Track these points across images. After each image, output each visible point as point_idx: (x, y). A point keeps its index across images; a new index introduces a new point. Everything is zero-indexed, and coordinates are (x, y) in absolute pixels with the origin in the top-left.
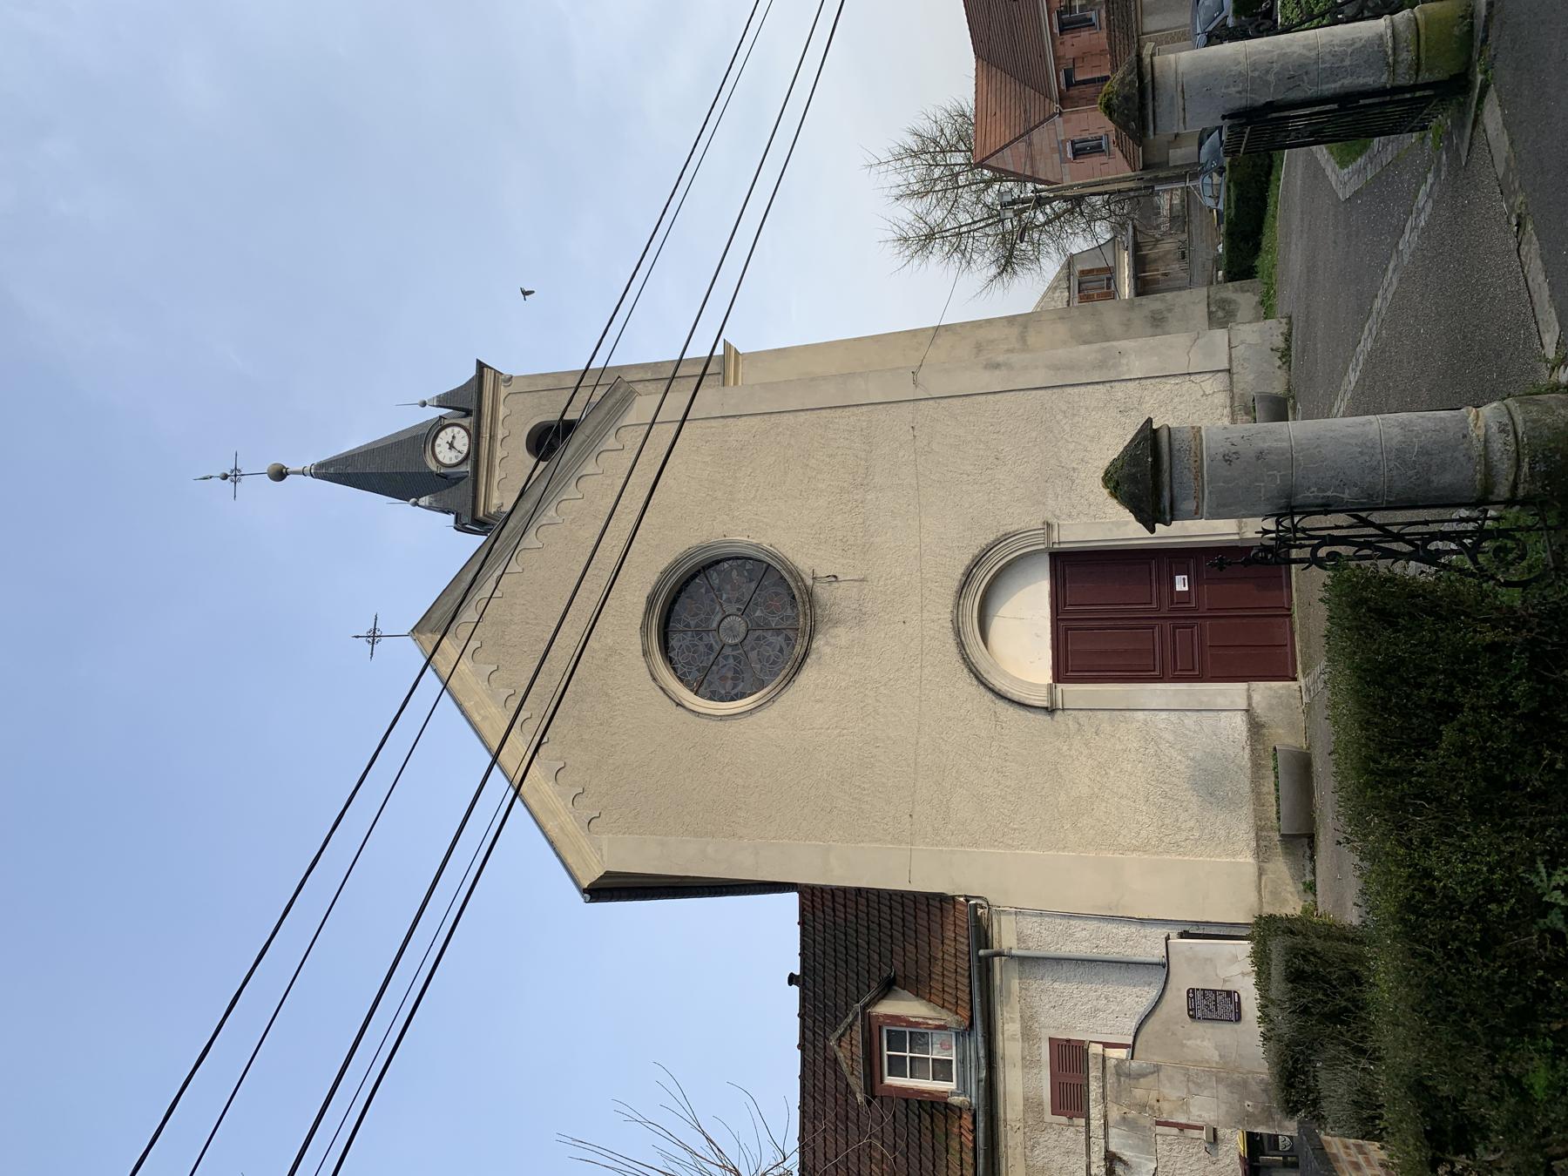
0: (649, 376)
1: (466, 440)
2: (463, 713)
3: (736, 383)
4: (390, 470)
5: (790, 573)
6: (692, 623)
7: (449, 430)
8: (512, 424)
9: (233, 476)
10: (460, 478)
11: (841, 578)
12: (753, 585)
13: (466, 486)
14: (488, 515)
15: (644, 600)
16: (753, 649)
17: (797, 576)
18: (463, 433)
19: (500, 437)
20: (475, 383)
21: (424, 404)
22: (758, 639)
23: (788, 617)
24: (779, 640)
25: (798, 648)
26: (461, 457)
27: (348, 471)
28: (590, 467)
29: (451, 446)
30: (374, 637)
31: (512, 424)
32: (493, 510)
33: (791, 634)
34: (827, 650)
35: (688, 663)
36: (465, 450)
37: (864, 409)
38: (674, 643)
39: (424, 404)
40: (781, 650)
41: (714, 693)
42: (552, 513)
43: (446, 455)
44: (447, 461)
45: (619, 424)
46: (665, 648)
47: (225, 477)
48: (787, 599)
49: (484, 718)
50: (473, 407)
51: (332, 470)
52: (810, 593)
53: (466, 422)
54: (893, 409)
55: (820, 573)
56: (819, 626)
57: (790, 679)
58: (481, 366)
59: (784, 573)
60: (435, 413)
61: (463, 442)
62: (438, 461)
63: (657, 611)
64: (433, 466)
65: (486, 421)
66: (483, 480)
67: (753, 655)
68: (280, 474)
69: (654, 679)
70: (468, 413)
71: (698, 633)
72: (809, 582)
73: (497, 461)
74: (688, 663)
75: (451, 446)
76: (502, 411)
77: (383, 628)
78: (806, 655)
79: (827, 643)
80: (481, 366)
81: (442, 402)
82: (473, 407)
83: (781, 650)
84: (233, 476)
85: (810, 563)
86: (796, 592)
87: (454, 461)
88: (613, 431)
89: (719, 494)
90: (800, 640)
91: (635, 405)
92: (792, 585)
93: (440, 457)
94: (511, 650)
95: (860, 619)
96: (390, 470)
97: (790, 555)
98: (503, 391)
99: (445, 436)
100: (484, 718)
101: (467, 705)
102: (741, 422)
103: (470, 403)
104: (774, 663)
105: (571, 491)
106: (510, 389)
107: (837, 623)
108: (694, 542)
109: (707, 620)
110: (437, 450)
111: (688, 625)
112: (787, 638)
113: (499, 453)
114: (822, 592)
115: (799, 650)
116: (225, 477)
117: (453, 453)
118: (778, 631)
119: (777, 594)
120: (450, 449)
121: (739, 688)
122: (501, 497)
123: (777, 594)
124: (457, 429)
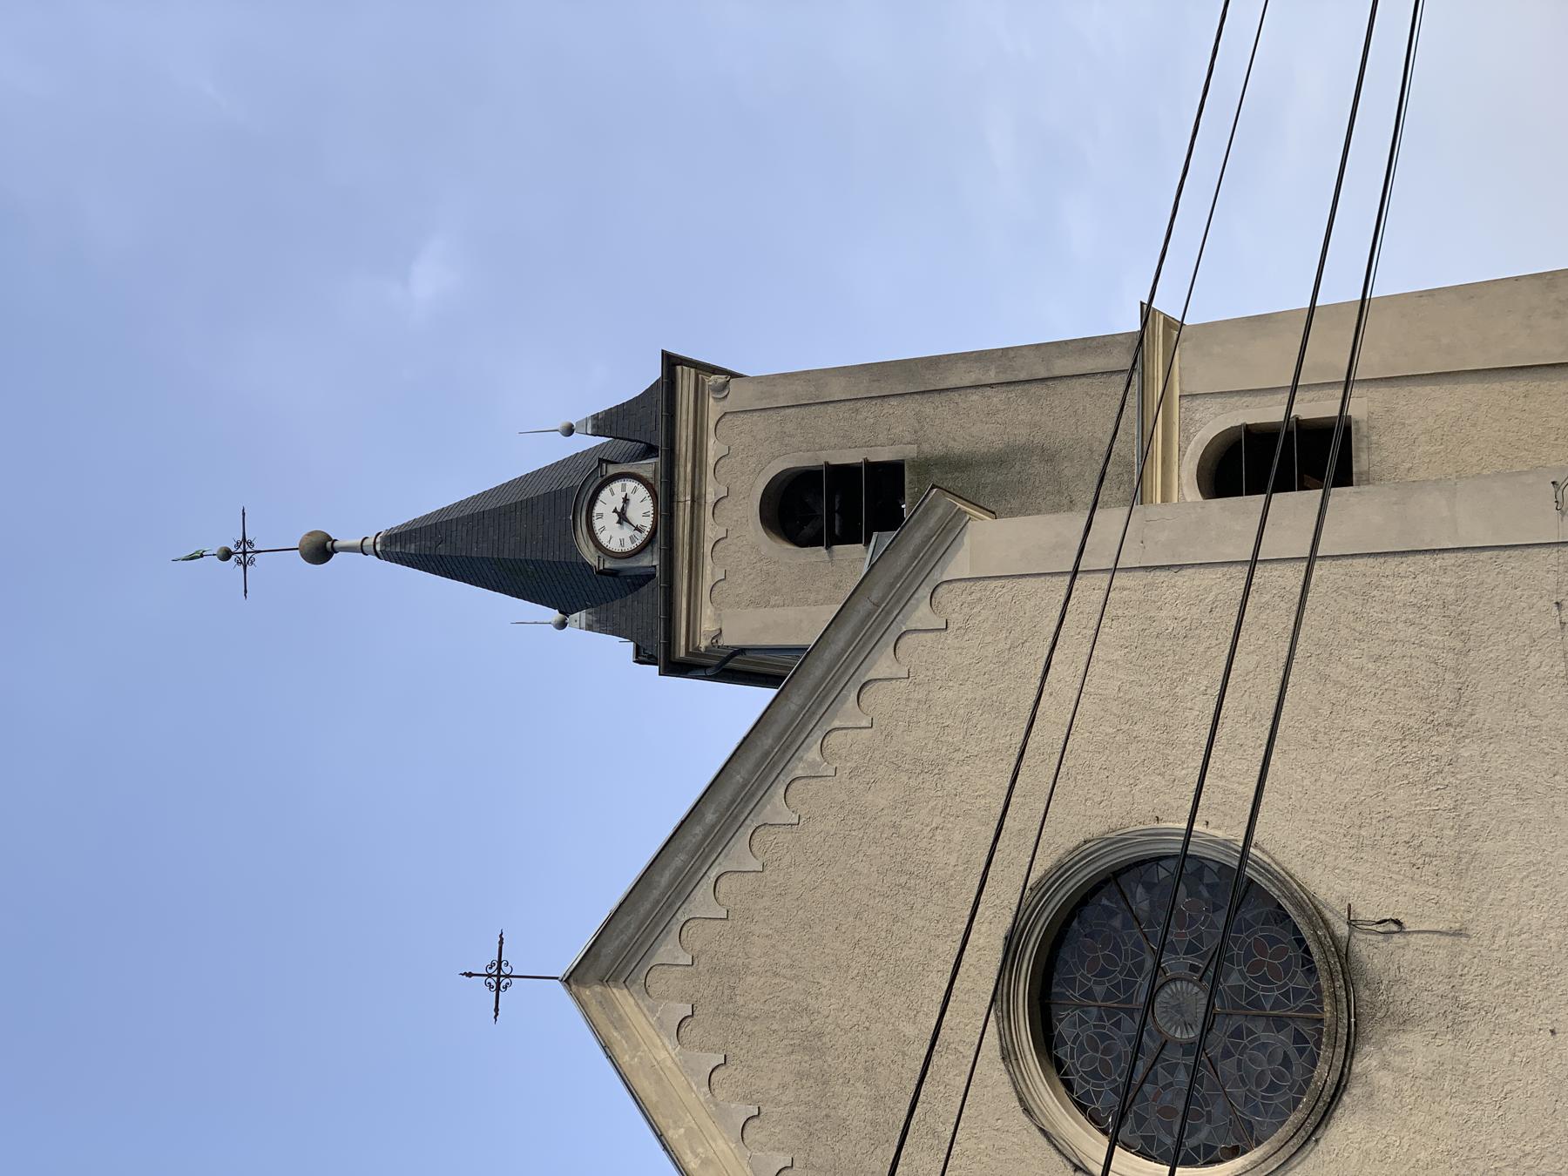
0: (992, 377)
1: (648, 506)
2: (665, 1148)
3: (1164, 500)
4: (511, 545)
5: (1299, 905)
6: (1099, 990)
7: (617, 486)
8: (736, 467)
9: (241, 553)
10: (646, 577)
11: (1409, 925)
12: (1220, 919)
13: (652, 594)
14: (694, 652)
15: (999, 945)
16: (1227, 1054)
17: (1316, 916)
18: (642, 492)
19: (710, 498)
20: (660, 396)
21: (569, 431)
22: (1237, 1033)
23: (1298, 993)
24: (1281, 1040)
25: (1322, 1069)
26: (641, 538)
27: (450, 546)
28: (882, 665)
29: (622, 517)
30: (498, 977)
31: (736, 467)
32: (703, 644)
33: (1307, 1030)
34: (1385, 1079)
35: (1094, 1074)
36: (647, 523)
37: (1449, 559)
38: (1063, 1028)
39: (569, 431)
40: (1286, 1062)
41: (1148, 1140)
42: (813, 754)
43: (615, 537)
44: (614, 546)
45: (937, 576)
46: (1046, 1041)
47: (226, 555)
48: (1294, 953)
49: (706, 1163)
50: (660, 441)
51: (412, 548)
52: (1343, 954)
53: (648, 467)
54: (1512, 561)
55: (1365, 913)
56: (1367, 1027)
57: (1325, 1114)
58: (671, 362)
59: (1284, 902)
60: (585, 442)
61: (642, 509)
62: (598, 545)
63: (1026, 966)
64: (590, 555)
65: (684, 469)
66: (682, 586)
67: (1227, 1067)
68: (320, 550)
69: (1027, 1111)
70: (650, 451)
71: (1111, 1012)
72: (1342, 930)
73: (708, 547)
74: (1094, 1074)
75: (622, 517)
76: (713, 449)
77: (516, 961)
78: (1340, 1088)
79: (1385, 1065)
80: (671, 362)
81: (604, 423)
82: (660, 441)
83: (1286, 1062)
84: (241, 553)
85: (1341, 888)
86: (1313, 948)
87: (629, 546)
88: (925, 591)
89: (1142, 730)
90: (1325, 1052)
91: (967, 539)
92: (1306, 932)
93: (603, 538)
94: (749, 1027)
95: (1456, 1018)
96: (511, 545)
97: (1296, 867)
98: (714, 409)
99: (609, 500)
100: (706, 1163)
101: (672, 1135)
102: (1183, 580)
103: (651, 428)
104: (1273, 1087)
105: (847, 712)
106: (726, 406)
107: (1405, 1022)
108: (1096, 829)
109: (1129, 985)
110: (598, 524)
111: (1089, 994)
112: (1299, 1038)
113: (711, 532)
114: (1370, 952)
115: (1324, 1074)
116: (226, 555)
117: (627, 532)
118: (1279, 1023)
119: (1273, 941)
120: (620, 520)
121: (1202, 1136)
122: (718, 617)
123: (1273, 941)
124: (631, 484)
